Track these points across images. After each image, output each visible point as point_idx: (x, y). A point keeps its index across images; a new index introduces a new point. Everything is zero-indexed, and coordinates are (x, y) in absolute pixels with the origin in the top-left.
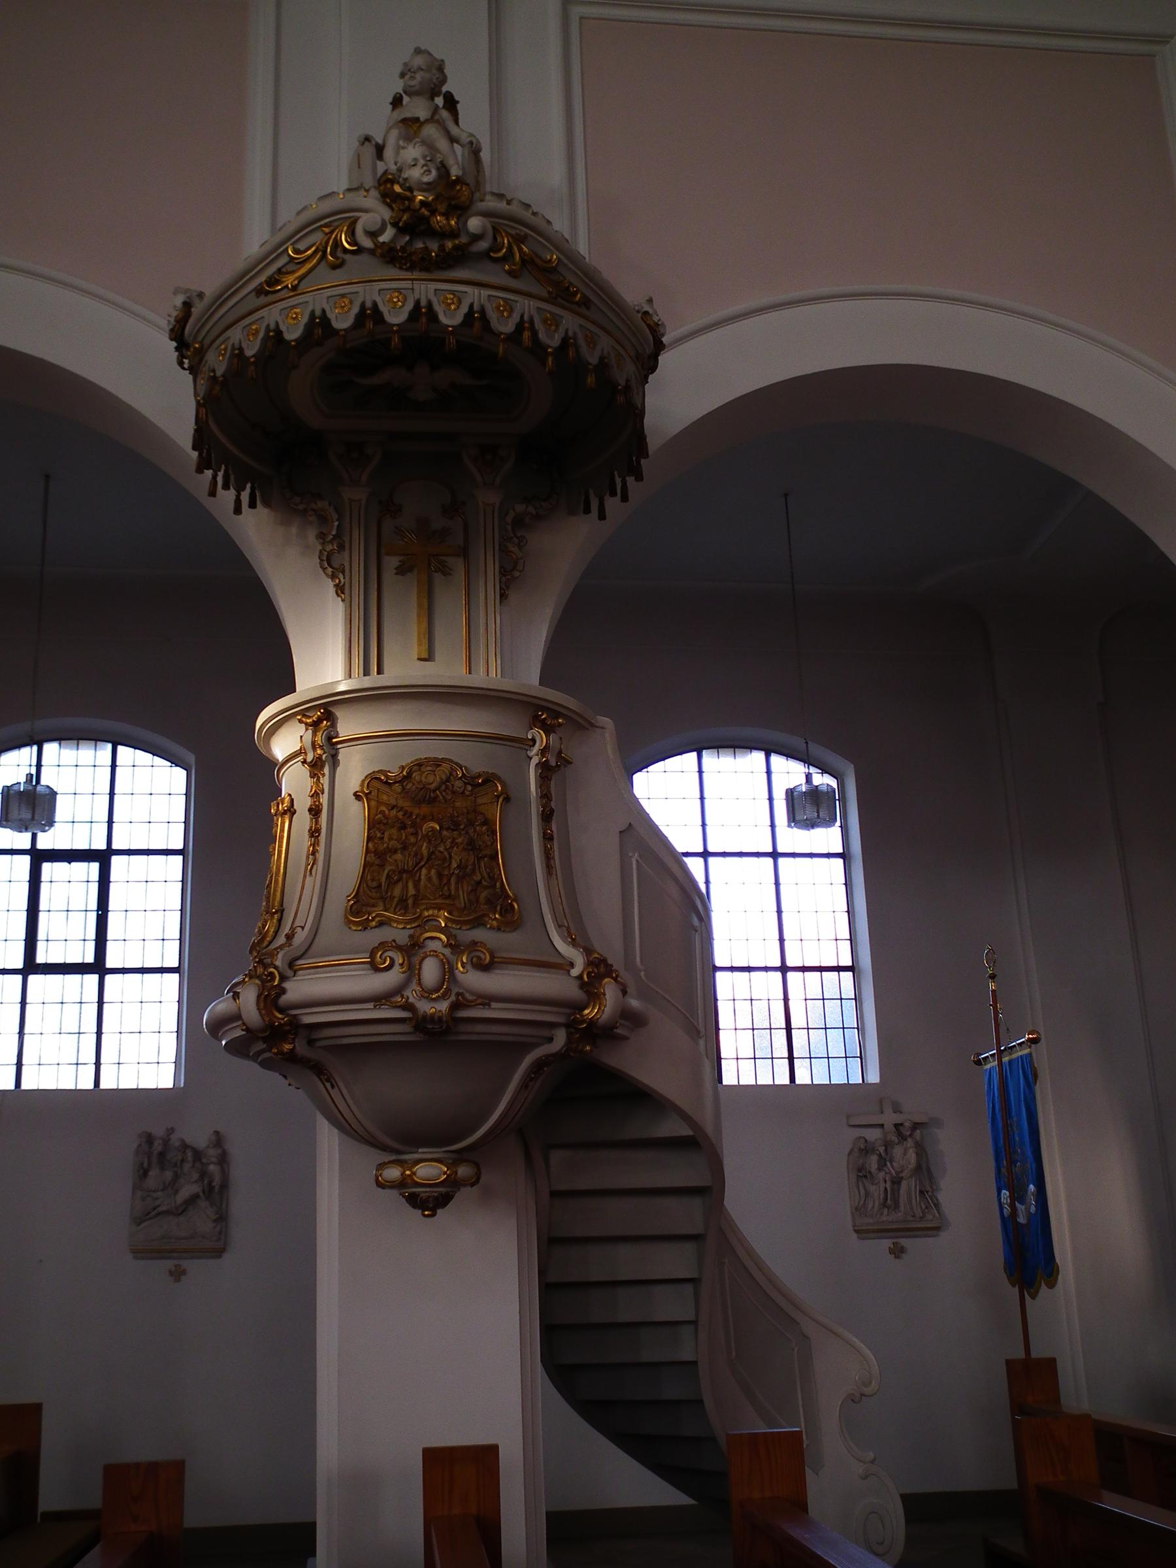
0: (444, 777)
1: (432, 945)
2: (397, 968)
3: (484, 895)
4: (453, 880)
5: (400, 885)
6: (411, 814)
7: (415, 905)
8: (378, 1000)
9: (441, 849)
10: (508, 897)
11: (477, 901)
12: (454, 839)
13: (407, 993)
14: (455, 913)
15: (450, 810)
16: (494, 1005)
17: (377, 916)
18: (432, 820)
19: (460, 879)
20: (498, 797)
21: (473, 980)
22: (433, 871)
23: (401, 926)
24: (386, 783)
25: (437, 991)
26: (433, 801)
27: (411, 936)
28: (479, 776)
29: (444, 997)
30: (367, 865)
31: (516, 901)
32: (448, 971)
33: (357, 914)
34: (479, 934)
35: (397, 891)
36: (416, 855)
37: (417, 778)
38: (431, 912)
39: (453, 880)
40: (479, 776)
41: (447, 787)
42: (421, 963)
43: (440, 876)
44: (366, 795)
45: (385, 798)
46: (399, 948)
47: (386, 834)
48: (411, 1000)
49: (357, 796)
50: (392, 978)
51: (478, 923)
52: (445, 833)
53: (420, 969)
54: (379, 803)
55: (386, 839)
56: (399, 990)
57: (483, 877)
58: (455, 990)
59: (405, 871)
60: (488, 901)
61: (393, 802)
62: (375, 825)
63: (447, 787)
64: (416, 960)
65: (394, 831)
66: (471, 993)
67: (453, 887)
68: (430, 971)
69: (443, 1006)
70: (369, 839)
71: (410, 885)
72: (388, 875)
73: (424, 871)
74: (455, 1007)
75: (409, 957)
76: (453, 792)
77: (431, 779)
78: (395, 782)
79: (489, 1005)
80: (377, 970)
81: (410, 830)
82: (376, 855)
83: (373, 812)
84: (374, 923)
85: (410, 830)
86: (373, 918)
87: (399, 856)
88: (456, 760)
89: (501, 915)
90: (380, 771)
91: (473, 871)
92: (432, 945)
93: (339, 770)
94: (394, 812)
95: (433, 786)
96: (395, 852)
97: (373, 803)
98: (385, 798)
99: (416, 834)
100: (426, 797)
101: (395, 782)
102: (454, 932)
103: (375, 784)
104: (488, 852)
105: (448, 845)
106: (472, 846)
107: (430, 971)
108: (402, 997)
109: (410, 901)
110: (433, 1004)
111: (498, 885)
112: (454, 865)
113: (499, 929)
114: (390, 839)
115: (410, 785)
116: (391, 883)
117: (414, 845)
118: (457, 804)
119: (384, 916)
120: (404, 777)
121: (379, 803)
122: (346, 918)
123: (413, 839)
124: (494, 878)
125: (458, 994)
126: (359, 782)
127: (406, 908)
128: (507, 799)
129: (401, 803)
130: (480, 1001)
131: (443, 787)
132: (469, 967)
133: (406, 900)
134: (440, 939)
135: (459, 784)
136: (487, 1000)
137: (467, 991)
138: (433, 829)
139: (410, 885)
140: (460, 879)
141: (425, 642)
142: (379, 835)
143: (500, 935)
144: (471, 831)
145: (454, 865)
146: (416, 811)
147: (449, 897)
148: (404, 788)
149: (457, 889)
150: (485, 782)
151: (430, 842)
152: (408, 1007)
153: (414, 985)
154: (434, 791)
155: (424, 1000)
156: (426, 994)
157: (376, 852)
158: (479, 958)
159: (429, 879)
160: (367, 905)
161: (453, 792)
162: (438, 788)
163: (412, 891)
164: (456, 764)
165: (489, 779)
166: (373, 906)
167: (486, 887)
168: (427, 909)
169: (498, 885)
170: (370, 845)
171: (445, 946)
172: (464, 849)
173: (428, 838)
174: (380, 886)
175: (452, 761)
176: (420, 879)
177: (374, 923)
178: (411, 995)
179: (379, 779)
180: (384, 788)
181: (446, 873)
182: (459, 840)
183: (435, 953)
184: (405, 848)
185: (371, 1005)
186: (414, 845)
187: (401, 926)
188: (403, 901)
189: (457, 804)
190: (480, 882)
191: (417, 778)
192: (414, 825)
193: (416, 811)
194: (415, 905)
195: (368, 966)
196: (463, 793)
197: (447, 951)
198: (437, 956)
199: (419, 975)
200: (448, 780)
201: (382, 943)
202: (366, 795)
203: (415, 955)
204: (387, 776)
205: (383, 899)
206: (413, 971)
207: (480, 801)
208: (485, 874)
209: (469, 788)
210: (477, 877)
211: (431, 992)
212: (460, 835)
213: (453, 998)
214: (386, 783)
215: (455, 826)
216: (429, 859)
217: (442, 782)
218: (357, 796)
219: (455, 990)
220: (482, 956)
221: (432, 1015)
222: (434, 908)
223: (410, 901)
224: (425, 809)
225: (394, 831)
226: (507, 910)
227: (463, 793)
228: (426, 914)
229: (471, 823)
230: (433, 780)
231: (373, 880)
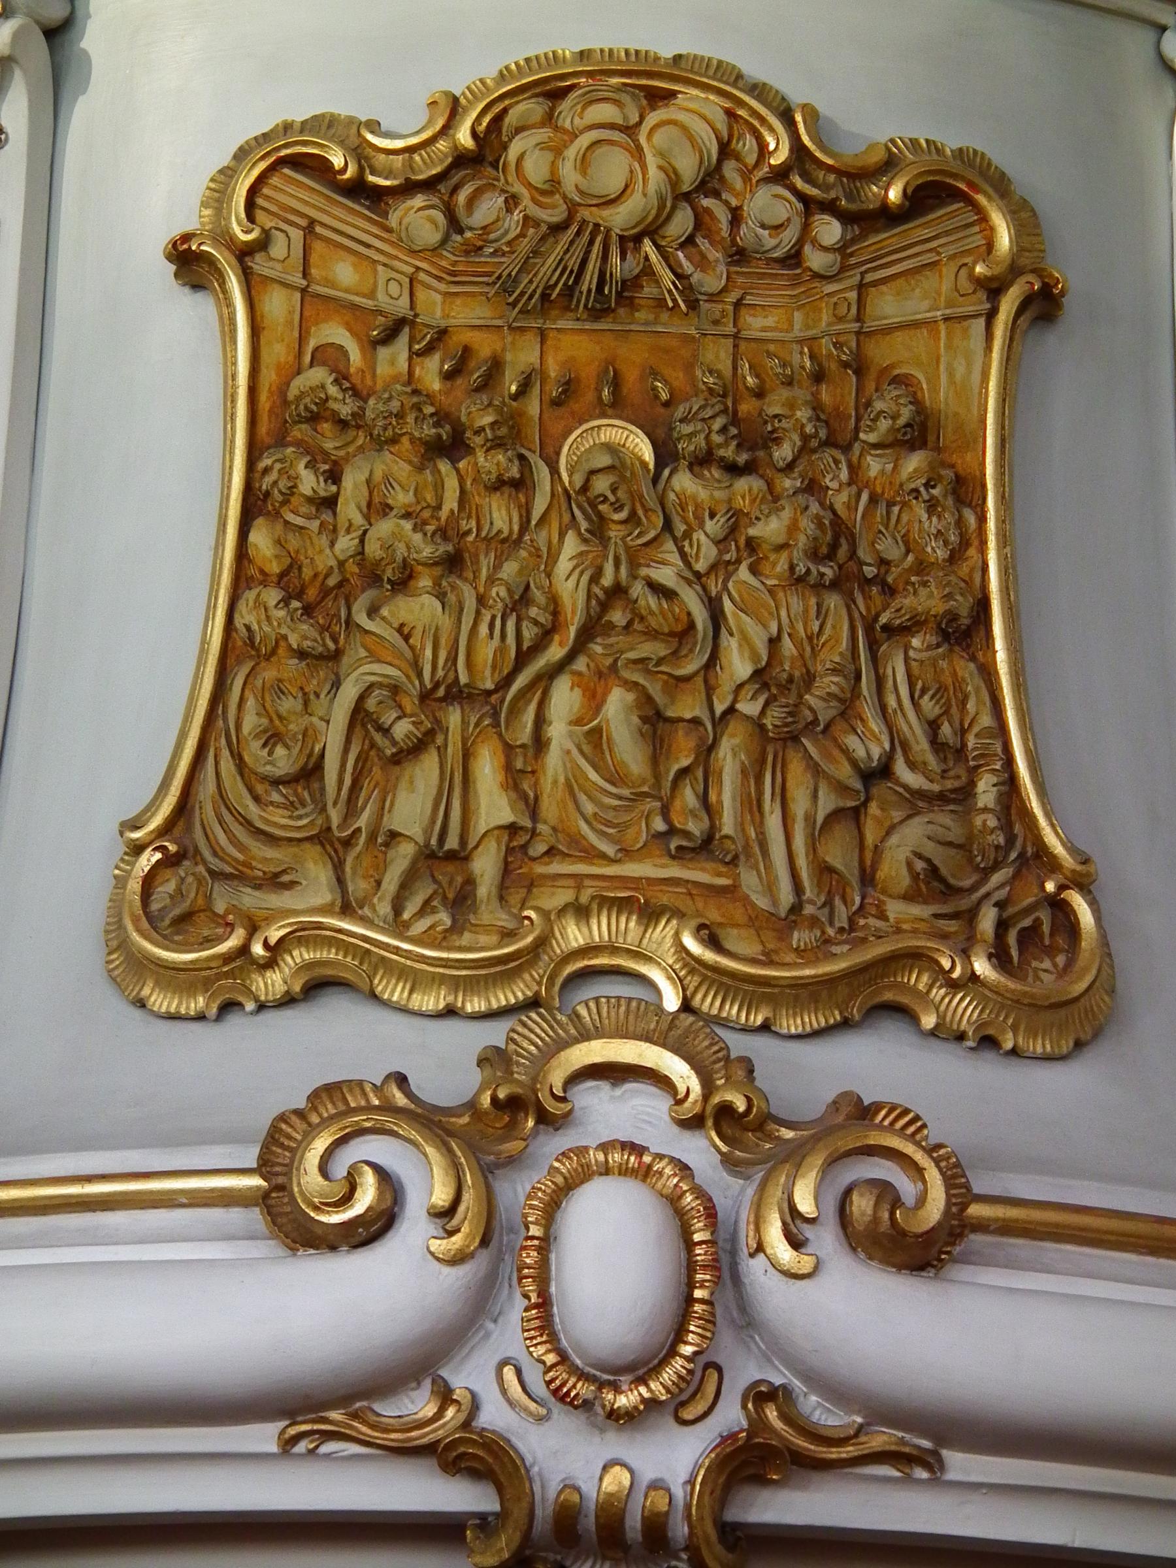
0: (688, 168)
1: (608, 1114)
2: (415, 1232)
3: (905, 843)
4: (730, 757)
5: (425, 774)
6: (496, 366)
7: (514, 879)
8: (310, 1410)
9: (666, 575)
10: (1051, 864)
11: (867, 878)
12: (736, 520)
13: (471, 1375)
14: (740, 941)
15: (718, 355)
16: (961, 1464)
17: (299, 936)
18: (617, 406)
19: (773, 745)
20: (994, 289)
21: (845, 1318)
22: (617, 705)
23: (431, 1001)
24: (358, 190)
25: (643, 1369)
26: (613, 300)
27: (494, 1060)
28: (889, 165)
29: (680, 1408)
30: (237, 650)
31: (1083, 884)
32: (706, 1270)
33: (181, 924)
34: (873, 1063)
35: (412, 806)
36: (520, 601)
37: (536, 169)
38: (600, 928)
39: (730, 757)
40: (889, 165)
41: (701, 222)
42: (552, 1207)
43: (654, 723)
44: (244, 254)
45: (345, 273)
46: (431, 1121)
47: (353, 481)
48: (494, 1416)
49: (188, 263)
50: (390, 1289)
51: (869, 999)
52: (684, 482)
53: (545, 1245)
54: (314, 301)
55: (350, 510)
56: (423, 1362)
57: (898, 742)
58: (745, 1370)
59: (457, 694)
60: (931, 883)
61: (392, 298)
62: (291, 433)
63: (701, 222)
64: (519, 1191)
65: (396, 466)
66: (837, 1392)
67: (727, 795)
68: (610, 1261)
69: (671, 1461)
70: (254, 505)
71: (487, 769)
72: (359, 715)
73: (564, 698)
74: (746, 1462)
75: (487, 1172)
76: (739, 256)
77: (612, 170)
78: (410, 188)
79: (931, 1462)
80: (300, 1234)
81: (489, 463)
82: (290, 601)
83: (277, 352)
84: (273, 983)
85: (489, 463)
86: (275, 950)
87: (420, 608)
88: (754, 70)
89: (1000, 957)
90: (324, 124)
91: (847, 708)
92: (608, 1114)
93: (85, 115)
94: (394, 359)
95: (620, 218)
96: (403, 582)
97: (278, 305)
98: (345, 273)
99: (518, 485)
100: (584, 276)
101: (410, 188)
102: (739, 1045)
103: (296, 193)
104: (928, 600)
105: (706, 554)
106: (837, 562)
107: (610, 1261)
108: (445, 1396)
109: (486, 865)
110: (615, 1444)
111: (986, 791)
112: (738, 665)
113: (988, 1042)
114: (376, 509)
115: (489, 208)
116: (380, 755)
117: (508, 544)
118: (756, 324)
119: (334, 940)
120: (461, 160)
121: (314, 301)
122: (117, 943)
123: (500, 515)
124: (961, 755)
125: (761, 1395)
126: (199, 183)
127: (461, 901)
128: (1044, 305)
129: (434, 306)
130: (881, 1438)
131: (681, 222)
132: (826, 1240)
133: (460, 857)
134: (662, 1081)
135: (768, 205)
136: (921, 1436)
137: (817, 1381)
138: (619, 463)
139: (487, 769)
140: (773, 745)
141: (193, 791)
142: (309, 482)
143: (989, 1073)
144: (835, 479)
145: (738, 665)
146: (523, 355)
147: (706, 846)
148: (455, 224)
149: (753, 806)
150: (930, 195)
151: (598, 531)
152: (474, 1454)
153: (509, 1333)
154: (630, 242)
155: (563, 1420)
156: (584, 1387)
157: (290, 582)
158: (885, 1191)
159: (595, 740)
160: (239, 877)
161: (739, 256)
162: (652, 230)
163: (494, 807)
164: (759, 90)
165: (943, 189)
166: (276, 881)
167: (917, 802)
168: (582, 912)
169: (986, 791)
170: (261, 539)
171: (694, 1123)
172: (797, 581)
173: (588, 509)
174: (310, 772)
175: (738, 78)
176: (540, 743)
177: (273, 983)
178: (493, 1384)
179: (317, 167)
180: (346, 218)
181: (688, 707)
182: (770, 529)
183: (632, 1161)
184: (453, 563)
185: (262, 1436)
186: (508, 544)
187: (431, 1001)
188: (443, 858)
189: (756, 324)
190: (878, 774)
191: (536, 169)
192: (509, 433)
193: (523, 355)
194: (514, 879)
195: (255, 1216)
196: (794, 258)
197: (701, 1151)
198: (645, 1174)
199: (543, 1278)
200: (710, 182)
201: (331, 1090)
202: (244, 254)
203: (512, 1161)
204: (360, 152)
205: (331, 844)
206: (509, 1256)
207: (888, 306)
208: (913, 727)
209: (830, 230)
210: (868, 745)
211: (612, 1373)
212: (773, 497)
213: (730, 1415)
214: (358, 190)
215: (747, 448)
216: (587, 634)
217: (680, 196)
218: (188, 263)
219: (745, 1370)
220: (907, 1187)
221: (611, 1517)
222: (622, 905)
223: (486, 865)
224: (574, 346)
225: (396, 466)
226: (1038, 934)
227: (794, 258)
228: (574, 935)
229: (834, 436)
230: (624, 179)
231: (272, 738)
